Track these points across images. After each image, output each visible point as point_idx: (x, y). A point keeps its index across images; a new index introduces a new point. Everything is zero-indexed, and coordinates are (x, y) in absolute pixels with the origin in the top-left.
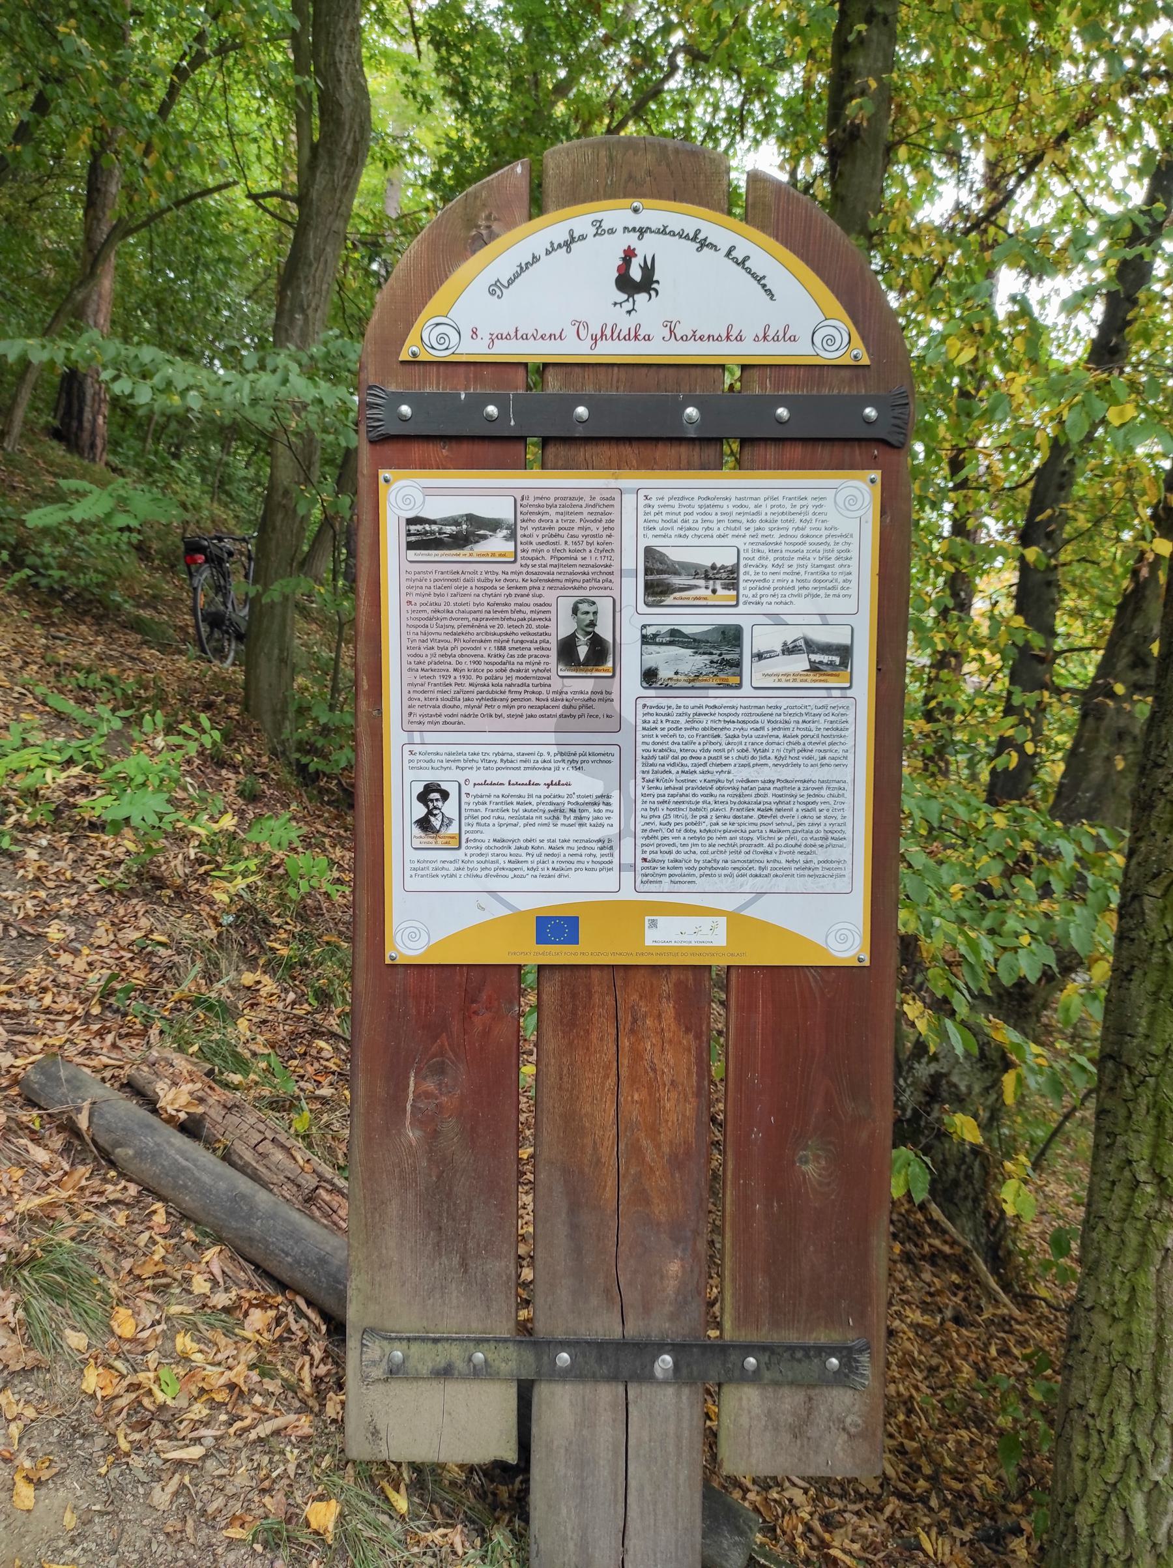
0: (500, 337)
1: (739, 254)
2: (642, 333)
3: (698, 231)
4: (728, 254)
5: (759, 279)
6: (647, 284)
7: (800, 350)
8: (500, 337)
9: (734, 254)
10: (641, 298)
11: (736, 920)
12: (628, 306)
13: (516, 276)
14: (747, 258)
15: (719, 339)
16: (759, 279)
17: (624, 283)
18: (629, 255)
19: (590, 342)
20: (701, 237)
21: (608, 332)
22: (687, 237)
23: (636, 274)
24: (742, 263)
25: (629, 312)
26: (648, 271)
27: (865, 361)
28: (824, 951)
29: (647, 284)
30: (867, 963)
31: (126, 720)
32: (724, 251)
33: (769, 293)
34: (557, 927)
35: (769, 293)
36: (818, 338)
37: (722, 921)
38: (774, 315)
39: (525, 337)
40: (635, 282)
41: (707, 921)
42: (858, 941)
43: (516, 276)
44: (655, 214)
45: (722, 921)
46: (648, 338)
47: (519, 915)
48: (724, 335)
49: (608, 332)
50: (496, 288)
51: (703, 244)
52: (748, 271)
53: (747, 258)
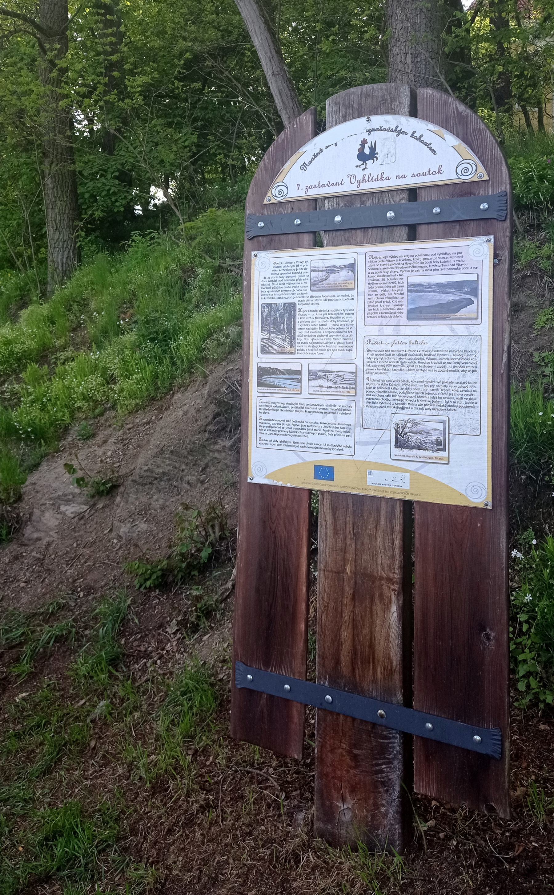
0: (311, 187)
1: (417, 135)
2: (385, 176)
3: (397, 127)
4: (412, 136)
5: (428, 145)
6: (373, 155)
7: (449, 175)
8: (311, 187)
9: (415, 135)
10: (369, 162)
11: (414, 475)
12: (363, 166)
13: (313, 160)
14: (422, 136)
15: (315, 187)
16: (428, 145)
17: (362, 157)
18: (364, 142)
19: (356, 184)
20: (398, 129)
21: (366, 178)
22: (392, 131)
23: (367, 151)
24: (419, 139)
25: (364, 169)
26: (373, 149)
27: (486, 178)
28: (467, 499)
29: (373, 155)
30: (490, 507)
31: (524, 709)
32: (410, 134)
33: (434, 152)
34: (324, 472)
35: (434, 152)
36: (459, 171)
37: (408, 475)
38: (432, 163)
39: (323, 186)
40: (366, 155)
41: (400, 474)
42: (484, 493)
43: (313, 160)
44: (378, 120)
45: (408, 475)
46: (388, 179)
47: (305, 463)
48: (437, 171)
49: (366, 178)
50: (304, 167)
51: (399, 132)
52: (422, 142)
53: (422, 136)
